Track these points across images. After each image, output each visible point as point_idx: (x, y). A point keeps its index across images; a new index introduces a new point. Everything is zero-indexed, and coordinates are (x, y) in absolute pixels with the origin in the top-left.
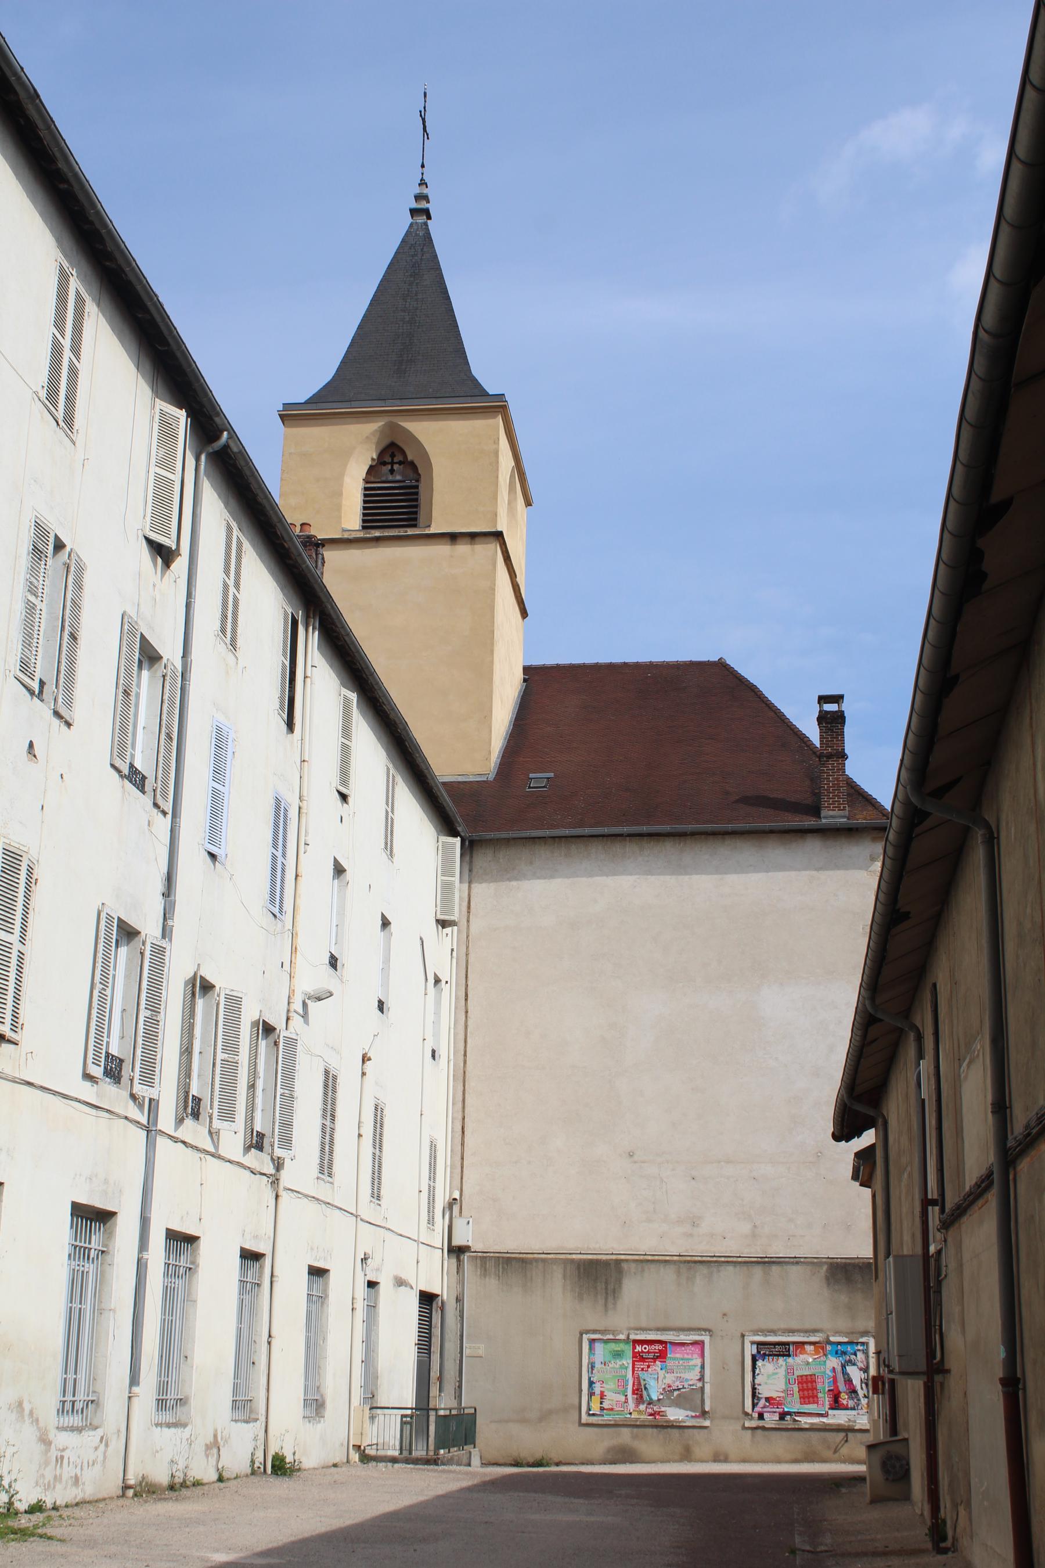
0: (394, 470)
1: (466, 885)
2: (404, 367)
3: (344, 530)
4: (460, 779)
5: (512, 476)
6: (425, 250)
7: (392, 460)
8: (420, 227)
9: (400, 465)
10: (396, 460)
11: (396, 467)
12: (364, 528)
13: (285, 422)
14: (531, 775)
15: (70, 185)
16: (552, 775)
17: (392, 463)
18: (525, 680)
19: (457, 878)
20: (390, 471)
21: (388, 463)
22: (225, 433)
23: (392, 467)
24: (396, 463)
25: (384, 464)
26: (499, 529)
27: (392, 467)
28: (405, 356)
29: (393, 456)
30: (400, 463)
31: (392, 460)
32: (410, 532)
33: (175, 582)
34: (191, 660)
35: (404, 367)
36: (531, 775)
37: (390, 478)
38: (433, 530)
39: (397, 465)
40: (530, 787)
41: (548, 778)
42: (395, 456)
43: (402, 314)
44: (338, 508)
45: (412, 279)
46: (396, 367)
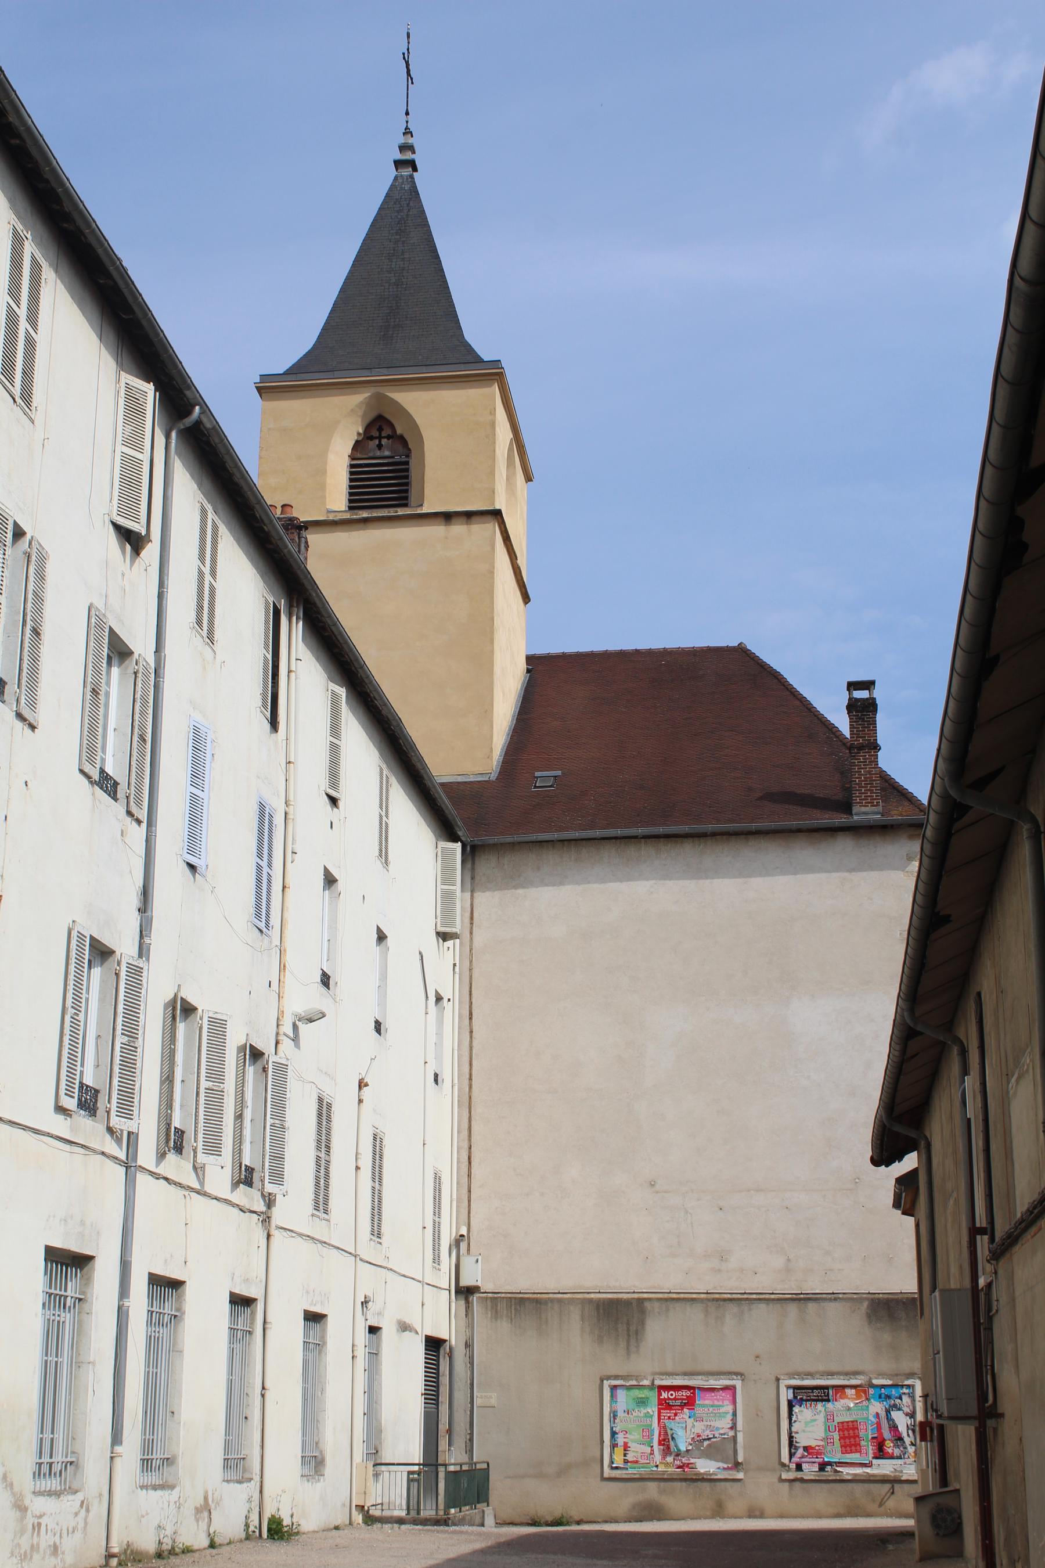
0: (378, 430)
1: (468, 895)
2: (390, 333)
3: (329, 512)
4: (460, 779)
5: (510, 449)
6: (411, 204)
7: (380, 434)
8: (405, 180)
9: (388, 439)
10: (384, 434)
11: (384, 442)
12: (350, 508)
13: (263, 395)
14: (537, 774)
15: (23, 141)
16: (559, 773)
17: (380, 438)
18: (528, 671)
19: (458, 887)
20: (378, 446)
21: (376, 438)
22: (197, 408)
23: (380, 441)
24: (384, 437)
25: (371, 438)
26: (497, 507)
27: (380, 441)
28: (392, 320)
29: (380, 430)
30: (388, 437)
31: (380, 434)
32: (401, 512)
33: (146, 570)
34: (165, 655)
35: (390, 333)
36: (537, 774)
37: (378, 453)
38: (425, 510)
39: (386, 440)
40: (535, 787)
41: (556, 777)
42: (383, 430)
43: (388, 275)
44: (322, 487)
45: (398, 237)
46: (382, 333)
